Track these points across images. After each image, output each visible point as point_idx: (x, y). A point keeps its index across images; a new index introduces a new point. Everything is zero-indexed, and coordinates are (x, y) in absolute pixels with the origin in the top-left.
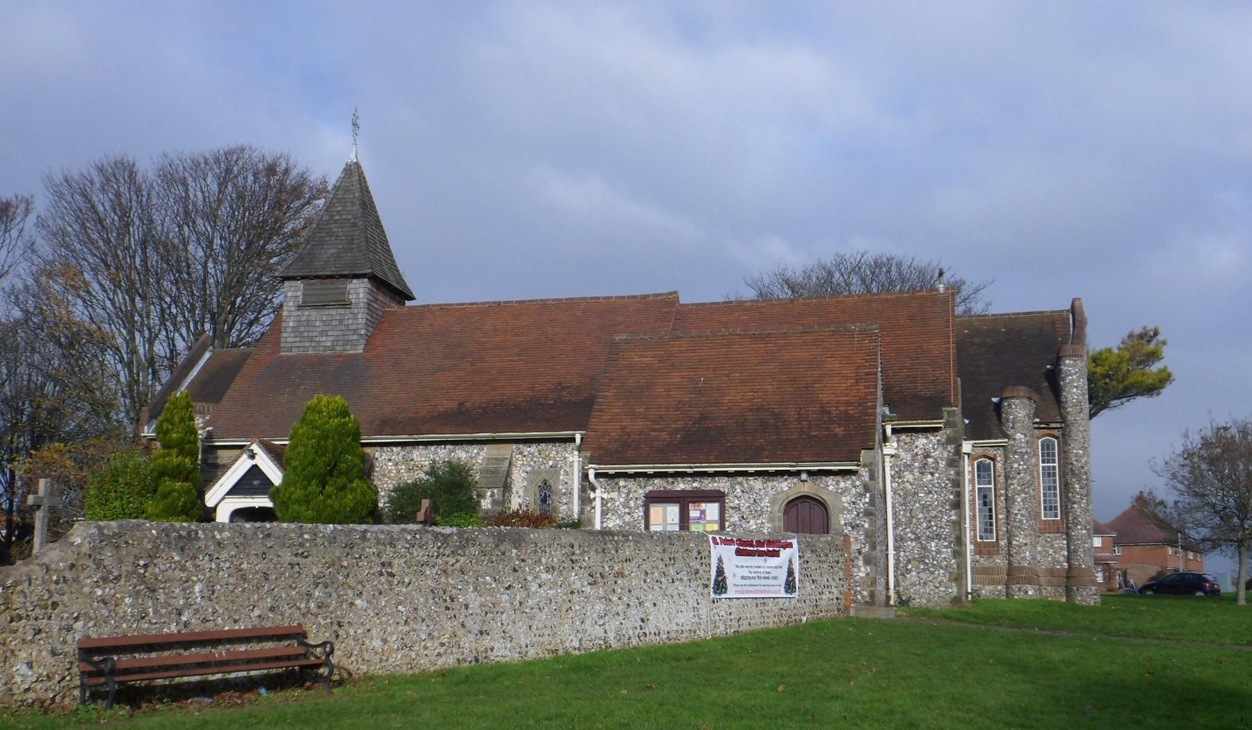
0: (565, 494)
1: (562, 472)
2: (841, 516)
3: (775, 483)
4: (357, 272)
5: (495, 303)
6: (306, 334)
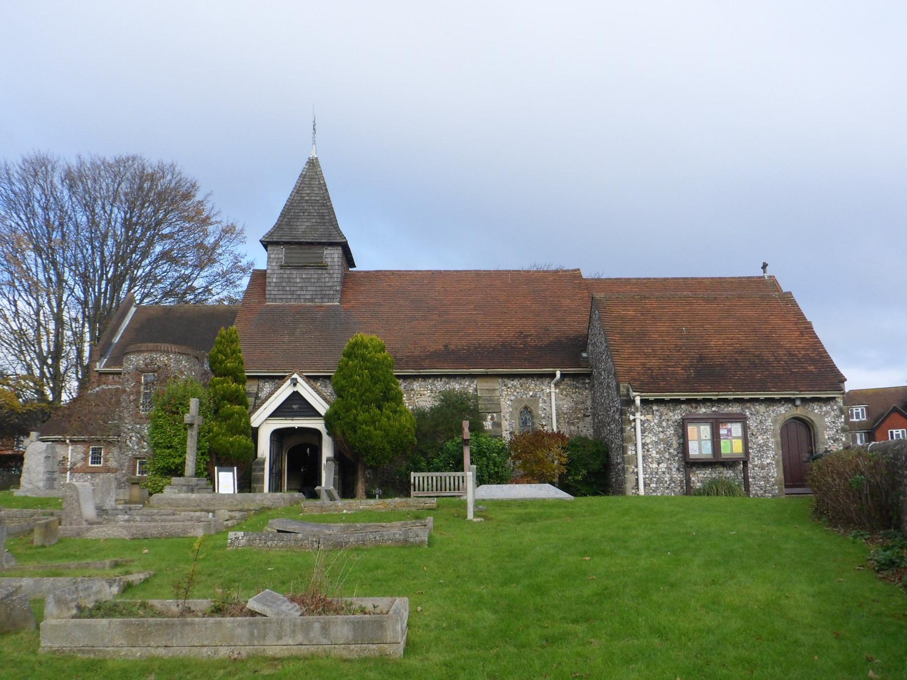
0: (544, 418)
1: (541, 400)
2: (825, 432)
3: (775, 407)
4: (333, 241)
5: (437, 271)
6: (288, 289)
